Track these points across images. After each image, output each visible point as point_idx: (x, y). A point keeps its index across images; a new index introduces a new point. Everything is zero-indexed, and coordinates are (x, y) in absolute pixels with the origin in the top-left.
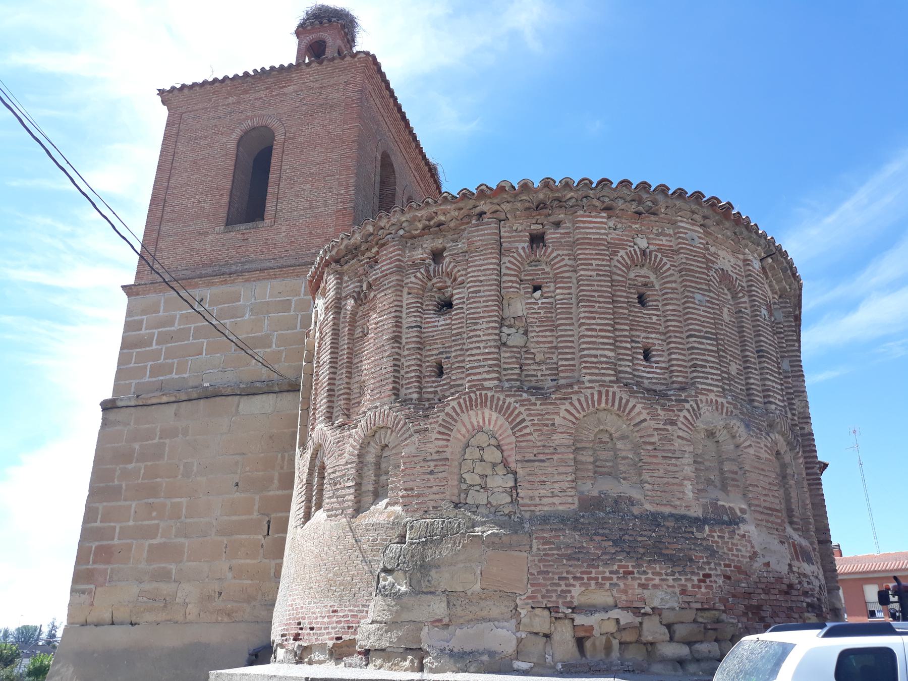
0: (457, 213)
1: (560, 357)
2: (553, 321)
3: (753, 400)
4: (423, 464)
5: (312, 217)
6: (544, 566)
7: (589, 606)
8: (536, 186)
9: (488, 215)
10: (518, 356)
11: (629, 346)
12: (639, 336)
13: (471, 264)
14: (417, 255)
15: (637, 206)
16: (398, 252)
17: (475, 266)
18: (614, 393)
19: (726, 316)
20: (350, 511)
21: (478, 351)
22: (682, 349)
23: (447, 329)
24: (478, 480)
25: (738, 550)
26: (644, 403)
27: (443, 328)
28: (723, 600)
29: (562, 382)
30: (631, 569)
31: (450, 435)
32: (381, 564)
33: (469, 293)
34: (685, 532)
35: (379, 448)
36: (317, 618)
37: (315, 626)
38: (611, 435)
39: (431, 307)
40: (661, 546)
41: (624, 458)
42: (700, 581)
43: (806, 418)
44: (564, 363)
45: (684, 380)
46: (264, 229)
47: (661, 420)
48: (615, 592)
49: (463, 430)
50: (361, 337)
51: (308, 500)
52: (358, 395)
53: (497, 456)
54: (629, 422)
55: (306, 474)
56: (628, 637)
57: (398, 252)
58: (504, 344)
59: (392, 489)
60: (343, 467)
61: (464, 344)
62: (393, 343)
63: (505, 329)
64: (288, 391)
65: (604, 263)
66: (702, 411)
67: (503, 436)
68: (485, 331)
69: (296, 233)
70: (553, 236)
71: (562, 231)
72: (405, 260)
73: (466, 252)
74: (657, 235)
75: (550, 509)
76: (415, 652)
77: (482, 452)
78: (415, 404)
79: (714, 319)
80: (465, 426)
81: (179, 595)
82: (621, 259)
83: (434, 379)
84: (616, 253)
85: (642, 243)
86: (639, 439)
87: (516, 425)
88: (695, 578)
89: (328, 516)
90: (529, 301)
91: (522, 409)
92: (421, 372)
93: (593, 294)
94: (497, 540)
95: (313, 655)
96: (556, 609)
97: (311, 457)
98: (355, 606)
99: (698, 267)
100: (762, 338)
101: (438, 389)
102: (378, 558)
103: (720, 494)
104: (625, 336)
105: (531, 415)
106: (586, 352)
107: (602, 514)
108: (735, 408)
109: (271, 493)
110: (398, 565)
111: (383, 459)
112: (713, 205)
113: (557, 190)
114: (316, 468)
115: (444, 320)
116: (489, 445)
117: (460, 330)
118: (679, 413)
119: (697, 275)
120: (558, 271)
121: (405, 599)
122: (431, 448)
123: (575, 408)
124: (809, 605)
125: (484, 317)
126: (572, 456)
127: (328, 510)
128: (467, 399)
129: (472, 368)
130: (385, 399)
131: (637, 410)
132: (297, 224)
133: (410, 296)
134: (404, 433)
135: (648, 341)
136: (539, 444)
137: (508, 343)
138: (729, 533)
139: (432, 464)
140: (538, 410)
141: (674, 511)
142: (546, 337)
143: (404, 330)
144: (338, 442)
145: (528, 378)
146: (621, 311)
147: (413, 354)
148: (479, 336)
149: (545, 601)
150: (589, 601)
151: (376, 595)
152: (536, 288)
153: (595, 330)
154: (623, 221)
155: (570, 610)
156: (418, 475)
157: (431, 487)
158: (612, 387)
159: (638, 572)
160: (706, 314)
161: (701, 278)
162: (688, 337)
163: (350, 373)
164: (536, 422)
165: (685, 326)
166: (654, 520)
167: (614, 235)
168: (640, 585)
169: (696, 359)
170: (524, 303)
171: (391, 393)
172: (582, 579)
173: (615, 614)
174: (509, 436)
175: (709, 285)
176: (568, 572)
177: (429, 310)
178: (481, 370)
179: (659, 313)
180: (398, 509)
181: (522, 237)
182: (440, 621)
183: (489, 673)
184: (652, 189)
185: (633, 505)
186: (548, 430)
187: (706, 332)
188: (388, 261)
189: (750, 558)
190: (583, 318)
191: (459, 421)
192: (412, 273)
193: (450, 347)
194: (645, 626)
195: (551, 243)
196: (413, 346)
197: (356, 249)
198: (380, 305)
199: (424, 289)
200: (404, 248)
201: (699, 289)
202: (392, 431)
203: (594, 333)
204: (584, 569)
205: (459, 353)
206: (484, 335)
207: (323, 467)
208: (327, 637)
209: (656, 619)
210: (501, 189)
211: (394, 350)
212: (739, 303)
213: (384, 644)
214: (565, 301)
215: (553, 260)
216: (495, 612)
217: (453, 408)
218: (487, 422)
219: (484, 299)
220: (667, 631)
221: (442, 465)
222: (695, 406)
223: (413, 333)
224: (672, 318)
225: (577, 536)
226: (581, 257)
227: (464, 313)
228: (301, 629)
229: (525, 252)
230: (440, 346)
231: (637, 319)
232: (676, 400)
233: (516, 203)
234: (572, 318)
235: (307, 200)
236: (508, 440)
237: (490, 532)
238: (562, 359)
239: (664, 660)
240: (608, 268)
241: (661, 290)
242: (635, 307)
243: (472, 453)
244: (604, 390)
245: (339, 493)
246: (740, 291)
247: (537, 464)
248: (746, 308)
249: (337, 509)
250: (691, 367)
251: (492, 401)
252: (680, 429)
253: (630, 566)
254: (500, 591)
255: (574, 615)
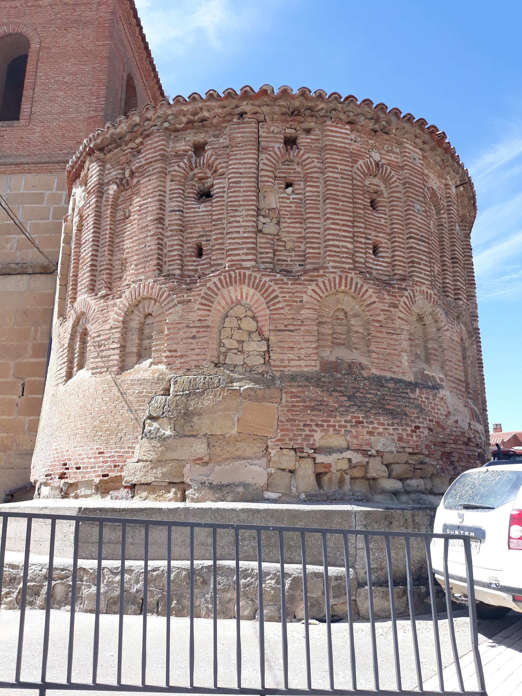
0: (220, 111)
1: (308, 245)
2: (302, 215)
4: (186, 330)
5: (65, 121)
6: (291, 415)
7: (327, 448)
8: (294, 93)
9: (249, 115)
10: (272, 242)
12: (370, 234)
13: (233, 157)
14: (180, 147)
15: (374, 125)
16: (163, 142)
17: (236, 159)
18: (352, 279)
20: (115, 369)
21: (237, 235)
22: (403, 248)
23: (207, 215)
24: (235, 345)
25: (438, 409)
26: (375, 289)
27: (204, 213)
28: (428, 447)
29: (309, 267)
30: (361, 419)
31: (211, 307)
33: (230, 183)
34: (402, 392)
36: (83, 459)
37: (81, 466)
38: (346, 313)
39: (192, 195)
40: (384, 402)
41: (356, 332)
42: (412, 431)
44: (311, 251)
45: (403, 273)
46: (19, 128)
47: (386, 303)
48: (348, 437)
49: (223, 303)
50: (123, 219)
51: (71, 361)
52: (120, 271)
53: (251, 325)
54: (362, 303)
55: (67, 339)
56: (357, 473)
57: (163, 142)
58: (260, 231)
59: (156, 351)
60: (108, 332)
61: (224, 228)
62: (157, 223)
63: (261, 218)
64: (41, 273)
65: (347, 168)
66: (417, 299)
67: (258, 309)
69: (49, 134)
70: (304, 140)
71: (313, 137)
72: (169, 150)
73: (227, 147)
74: (388, 151)
75: (298, 370)
76: (178, 485)
77: (239, 322)
78: (178, 279)
80: (224, 298)
82: (360, 167)
83: (194, 259)
84: (356, 162)
85: (377, 157)
86: (369, 317)
87: (270, 301)
88: (409, 429)
89: (93, 374)
90: (283, 195)
91: (276, 287)
92: (183, 252)
93: (338, 193)
94: (252, 393)
95: (79, 491)
96: (301, 450)
97: (73, 324)
98: (121, 448)
99: (418, 182)
100: (456, 248)
101: (199, 268)
102: (145, 408)
103: (425, 366)
104: (361, 232)
106: (330, 243)
107: (339, 375)
108: (439, 299)
109: (26, 360)
110: (163, 413)
111: (145, 326)
112: (432, 133)
113: (312, 99)
114: (77, 334)
115: (205, 207)
116: (246, 316)
117: (220, 216)
118: (400, 299)
119: (417, 189)
120: (308, 171)
121: (169, 441)
122: (194, 316)
123: (320, 289)
125: (244, 205)
126: (316, 328)
127: (93, 368)
128: (228, 277)
129: (232, 250)
130: (150, 273)
132: (51, 126)
133: (173, 183)
134: (168, 303)
135: (377, 239)
136: (289, 317)
137: (264, 230)
139: (194, 330)
140: (289, 288)
141: (394, 376)
142: (296, 228)
143: (167, 213)
144: (102, 310)
145: (280, 263)
146: (359, 211)
147: (176, 235)
148: (239, 222)
149: (292, 443)
150: (327, 444)
151: (142, 438)
155: (313, 451)
156: (182, 339)
157: (193, 349)
158: (351, 273)
159: (367, 422)
160: (422, 221)
162: (408, 238)
163: (112, 251)
164: (287, 298)
165: (406, 229)
167: (355, 146)
168: (368, 432)
169: (414, 257)
170: (277, 196)
171: (155, 268)
172: (323, 426)
173: (348, 454)
174: (263, 309)
176: (311, 420)
177: (190, 197)
178: (240, 252)
179: (386, 217)
180: (162, 367)
181: (278, 138)
182: (201, 459)
183: (244, 501)
184: (388, 110)
185: (363, 369)
186: (297, 306)
187: (421, 236)
188: (153, 150)
190: (329, 213)
191: (220, 295)
192: (175, 163)
193: (211, 231)
194: (370, 465)
195: (303, 146)
196: (176, 227)
197: (120, 139)
198: (144, 189)
199: (186, 177)
200: (167, 140)
201: (418, 200)
202: (156, 301)
203: (338, 227)
204: (324, 419)
205: (219, 236)
206: (243, 221)
207: (85, 333)
208: (94, 474)
209: (378, 459)
210: (264, 92)
211: (158, 230)
212: (442, 218)
213: (150, 479)
214: (314, 198)
215: (304, 161)
216: (249, 452)
217: (215, 283)
218: (244, 297)
219: (245, 189)
220: (386, 469)
221: (204, 331)
222: (412, 294)
223: (176, 216)
224: (397, 221)
225: (319, 392)
226: (329, 160)
227: (224, 201)
228: (67, 469)
229: (280, 151)
230: (200, 230)
231: (370, 220)
232: (398, 288)
233: (275, 107)
234: (319, 213)
235: (60, 106)
236: (263, 312)
237: (246, 387)
238: (310, 248)
239: (383, 492)
241: (388, 198)
242: (368, 209)
243: (233, 323)
244: (344, 275)
245: (104, 353)
247: (287, 333)
248: (445, 223)
249: (101, 367)
250: (409, 263)
251: (250, 279)
252: (400, 311)
253: (361, 416)
254: (254, 435)
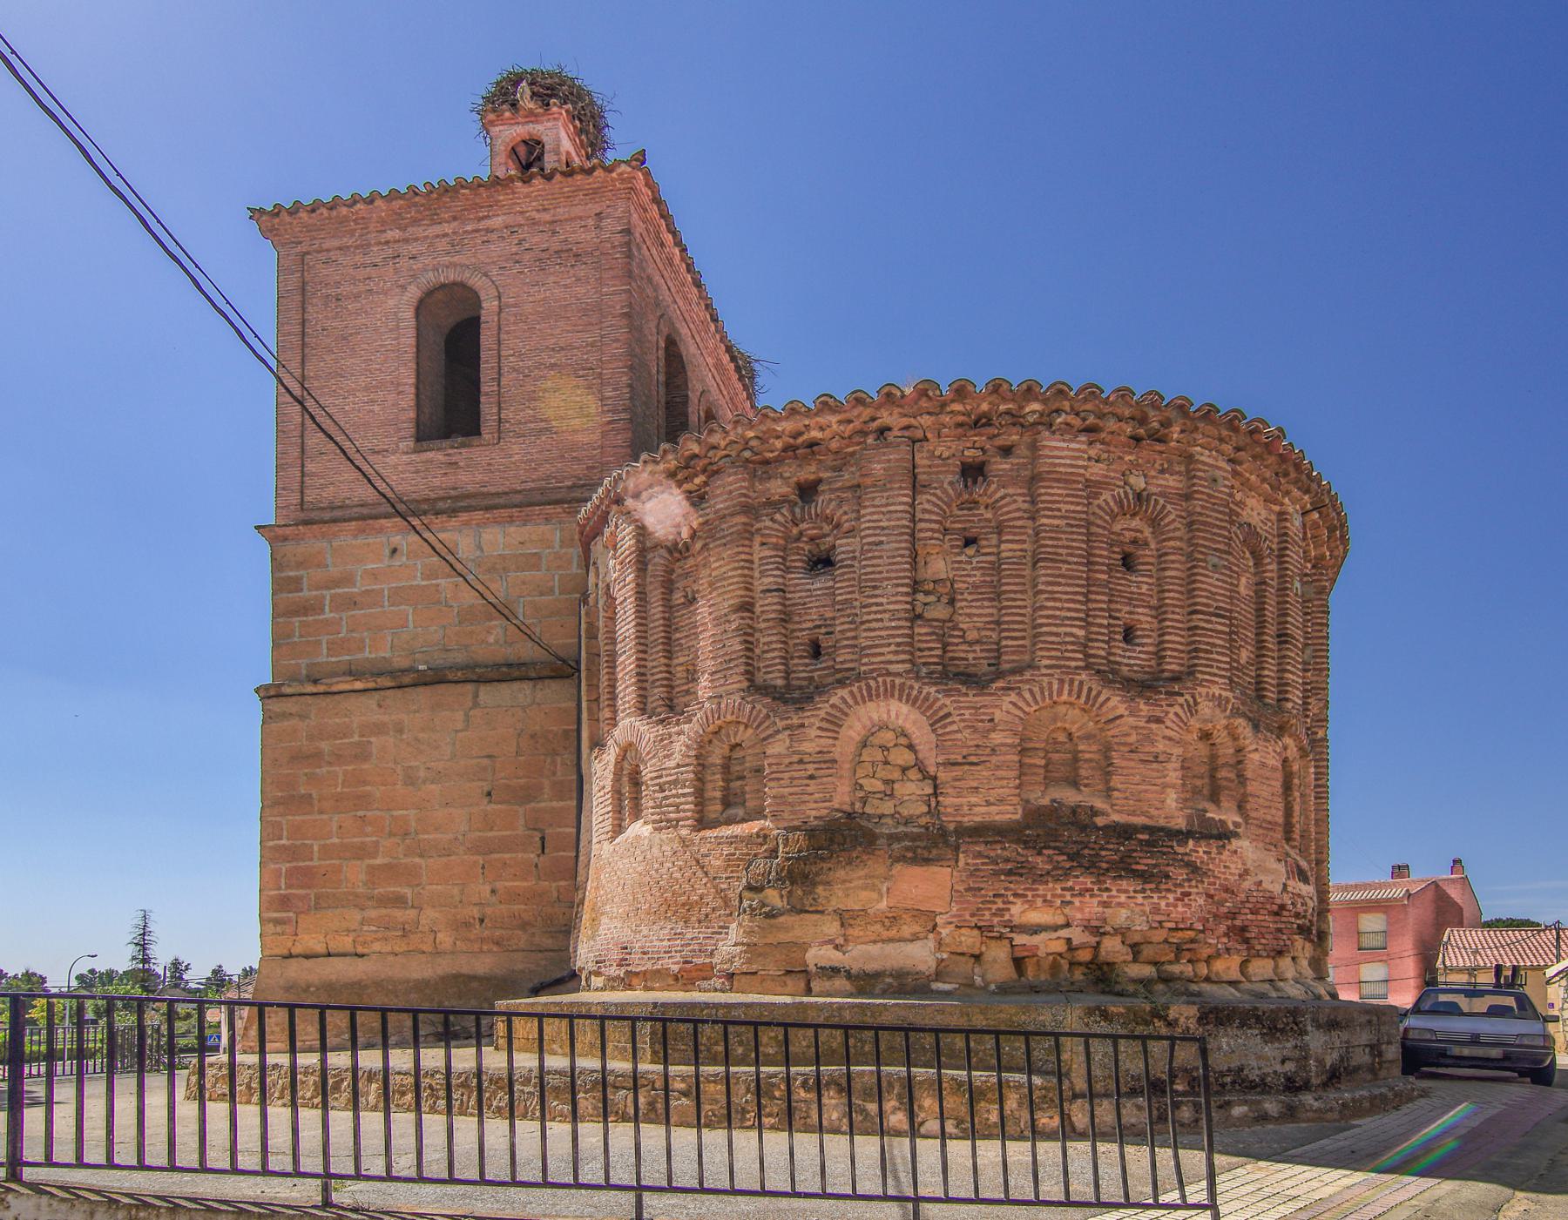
3: (1264, 696)
11: (1105, 622)
18: (1081, 683)
19: (1243, 590)
24: (879, 786)
28: (1205, 921)
30: (1089, 886)
32: (744, 880)
35: (727, 748)
42: (1177, 899)
43: (1322, 721)
63: (920, 596)
64: (551, 678)
65: (1079, 508)
66: (1199, 707)
68: (892, 598)
74: (1162, 471)
79: (1231, 591)
81: (423, 922)
82: (1103, 504)
83: (807, 661)
84: (1097, 495)
85: (1138, 482)
87: (938, 721)
89: (655, 829)
90: (959, 558)
91: (948, 701)
93: (1060, 551)
96: (990, 928)
101: (816, 674)
105: (960, 708)
116: (896, 745)
117: (849, 596)
118: (1169, 709)
124: (1299, 927)
131: (1111, 704)
136: (972, 743)
137: (925, 615)
138: (1218, 848)
144: (662, 740)
147: (774, 627)
148: (882, 604)
149: (974, 919)
152: (969, 542)
153: (1060, 600)
154: (1112, 449)
159: (1100, 889)
161: (1220, 535)
163: (669, 651)
164: (967, 717)
166: (1124, 832)
169: (1200, 642)
171: (742, 678)
172: (1026, 896)
175: (1229, 545)
177: (796, 567)
179: (1150, 581)
189: (1240, 876)
196: (773, 616)
203: (1058, 604)
209: (1118, 939)
215: (997, 501)
223: (773, 599)
232: (1166, 693)
240: (1084, 516)
241: (1158, 550)
242: (1117, 571)
246: (1269, 556)
247: (967, 767)
248: (1272, 579)
255: (1013, 935)
